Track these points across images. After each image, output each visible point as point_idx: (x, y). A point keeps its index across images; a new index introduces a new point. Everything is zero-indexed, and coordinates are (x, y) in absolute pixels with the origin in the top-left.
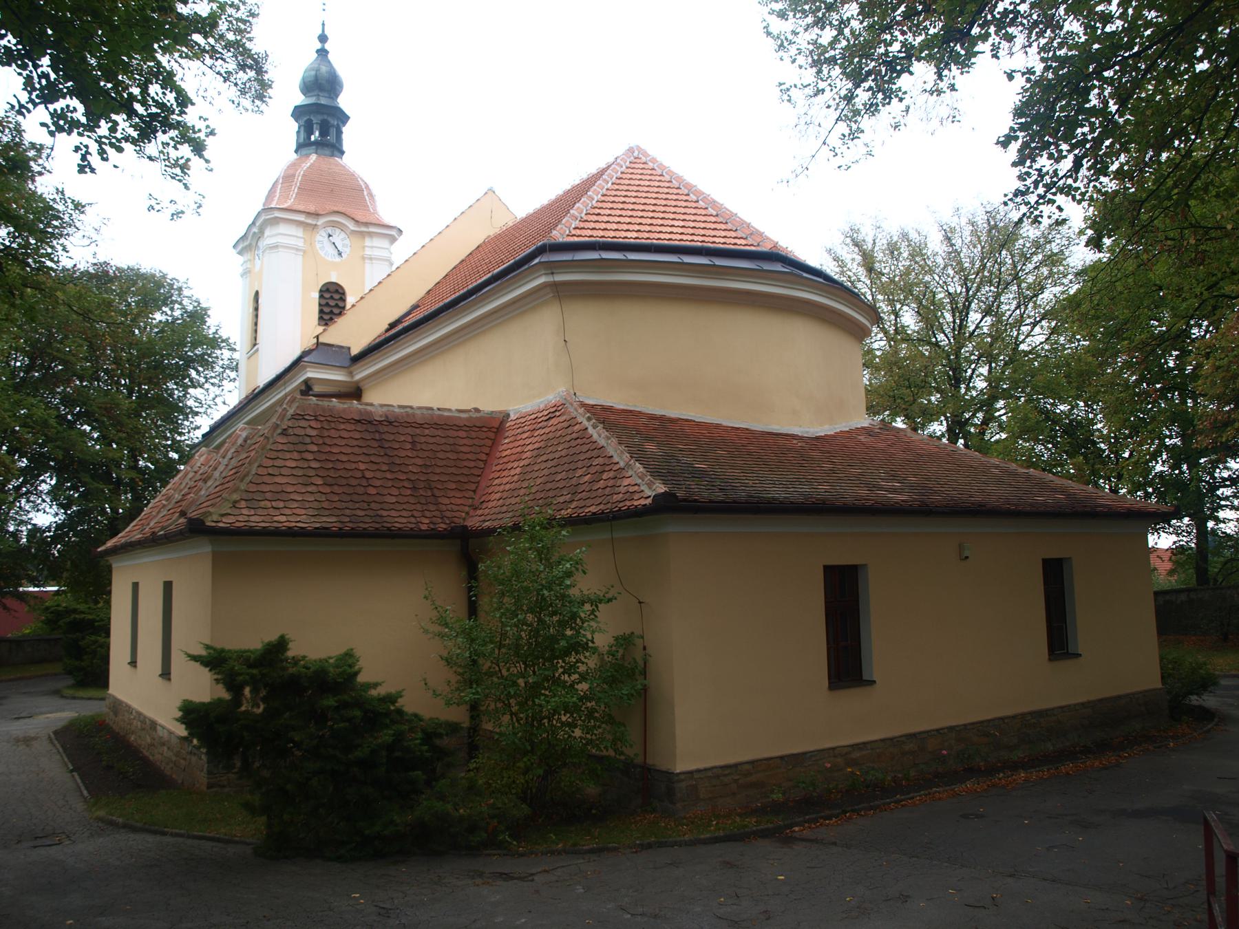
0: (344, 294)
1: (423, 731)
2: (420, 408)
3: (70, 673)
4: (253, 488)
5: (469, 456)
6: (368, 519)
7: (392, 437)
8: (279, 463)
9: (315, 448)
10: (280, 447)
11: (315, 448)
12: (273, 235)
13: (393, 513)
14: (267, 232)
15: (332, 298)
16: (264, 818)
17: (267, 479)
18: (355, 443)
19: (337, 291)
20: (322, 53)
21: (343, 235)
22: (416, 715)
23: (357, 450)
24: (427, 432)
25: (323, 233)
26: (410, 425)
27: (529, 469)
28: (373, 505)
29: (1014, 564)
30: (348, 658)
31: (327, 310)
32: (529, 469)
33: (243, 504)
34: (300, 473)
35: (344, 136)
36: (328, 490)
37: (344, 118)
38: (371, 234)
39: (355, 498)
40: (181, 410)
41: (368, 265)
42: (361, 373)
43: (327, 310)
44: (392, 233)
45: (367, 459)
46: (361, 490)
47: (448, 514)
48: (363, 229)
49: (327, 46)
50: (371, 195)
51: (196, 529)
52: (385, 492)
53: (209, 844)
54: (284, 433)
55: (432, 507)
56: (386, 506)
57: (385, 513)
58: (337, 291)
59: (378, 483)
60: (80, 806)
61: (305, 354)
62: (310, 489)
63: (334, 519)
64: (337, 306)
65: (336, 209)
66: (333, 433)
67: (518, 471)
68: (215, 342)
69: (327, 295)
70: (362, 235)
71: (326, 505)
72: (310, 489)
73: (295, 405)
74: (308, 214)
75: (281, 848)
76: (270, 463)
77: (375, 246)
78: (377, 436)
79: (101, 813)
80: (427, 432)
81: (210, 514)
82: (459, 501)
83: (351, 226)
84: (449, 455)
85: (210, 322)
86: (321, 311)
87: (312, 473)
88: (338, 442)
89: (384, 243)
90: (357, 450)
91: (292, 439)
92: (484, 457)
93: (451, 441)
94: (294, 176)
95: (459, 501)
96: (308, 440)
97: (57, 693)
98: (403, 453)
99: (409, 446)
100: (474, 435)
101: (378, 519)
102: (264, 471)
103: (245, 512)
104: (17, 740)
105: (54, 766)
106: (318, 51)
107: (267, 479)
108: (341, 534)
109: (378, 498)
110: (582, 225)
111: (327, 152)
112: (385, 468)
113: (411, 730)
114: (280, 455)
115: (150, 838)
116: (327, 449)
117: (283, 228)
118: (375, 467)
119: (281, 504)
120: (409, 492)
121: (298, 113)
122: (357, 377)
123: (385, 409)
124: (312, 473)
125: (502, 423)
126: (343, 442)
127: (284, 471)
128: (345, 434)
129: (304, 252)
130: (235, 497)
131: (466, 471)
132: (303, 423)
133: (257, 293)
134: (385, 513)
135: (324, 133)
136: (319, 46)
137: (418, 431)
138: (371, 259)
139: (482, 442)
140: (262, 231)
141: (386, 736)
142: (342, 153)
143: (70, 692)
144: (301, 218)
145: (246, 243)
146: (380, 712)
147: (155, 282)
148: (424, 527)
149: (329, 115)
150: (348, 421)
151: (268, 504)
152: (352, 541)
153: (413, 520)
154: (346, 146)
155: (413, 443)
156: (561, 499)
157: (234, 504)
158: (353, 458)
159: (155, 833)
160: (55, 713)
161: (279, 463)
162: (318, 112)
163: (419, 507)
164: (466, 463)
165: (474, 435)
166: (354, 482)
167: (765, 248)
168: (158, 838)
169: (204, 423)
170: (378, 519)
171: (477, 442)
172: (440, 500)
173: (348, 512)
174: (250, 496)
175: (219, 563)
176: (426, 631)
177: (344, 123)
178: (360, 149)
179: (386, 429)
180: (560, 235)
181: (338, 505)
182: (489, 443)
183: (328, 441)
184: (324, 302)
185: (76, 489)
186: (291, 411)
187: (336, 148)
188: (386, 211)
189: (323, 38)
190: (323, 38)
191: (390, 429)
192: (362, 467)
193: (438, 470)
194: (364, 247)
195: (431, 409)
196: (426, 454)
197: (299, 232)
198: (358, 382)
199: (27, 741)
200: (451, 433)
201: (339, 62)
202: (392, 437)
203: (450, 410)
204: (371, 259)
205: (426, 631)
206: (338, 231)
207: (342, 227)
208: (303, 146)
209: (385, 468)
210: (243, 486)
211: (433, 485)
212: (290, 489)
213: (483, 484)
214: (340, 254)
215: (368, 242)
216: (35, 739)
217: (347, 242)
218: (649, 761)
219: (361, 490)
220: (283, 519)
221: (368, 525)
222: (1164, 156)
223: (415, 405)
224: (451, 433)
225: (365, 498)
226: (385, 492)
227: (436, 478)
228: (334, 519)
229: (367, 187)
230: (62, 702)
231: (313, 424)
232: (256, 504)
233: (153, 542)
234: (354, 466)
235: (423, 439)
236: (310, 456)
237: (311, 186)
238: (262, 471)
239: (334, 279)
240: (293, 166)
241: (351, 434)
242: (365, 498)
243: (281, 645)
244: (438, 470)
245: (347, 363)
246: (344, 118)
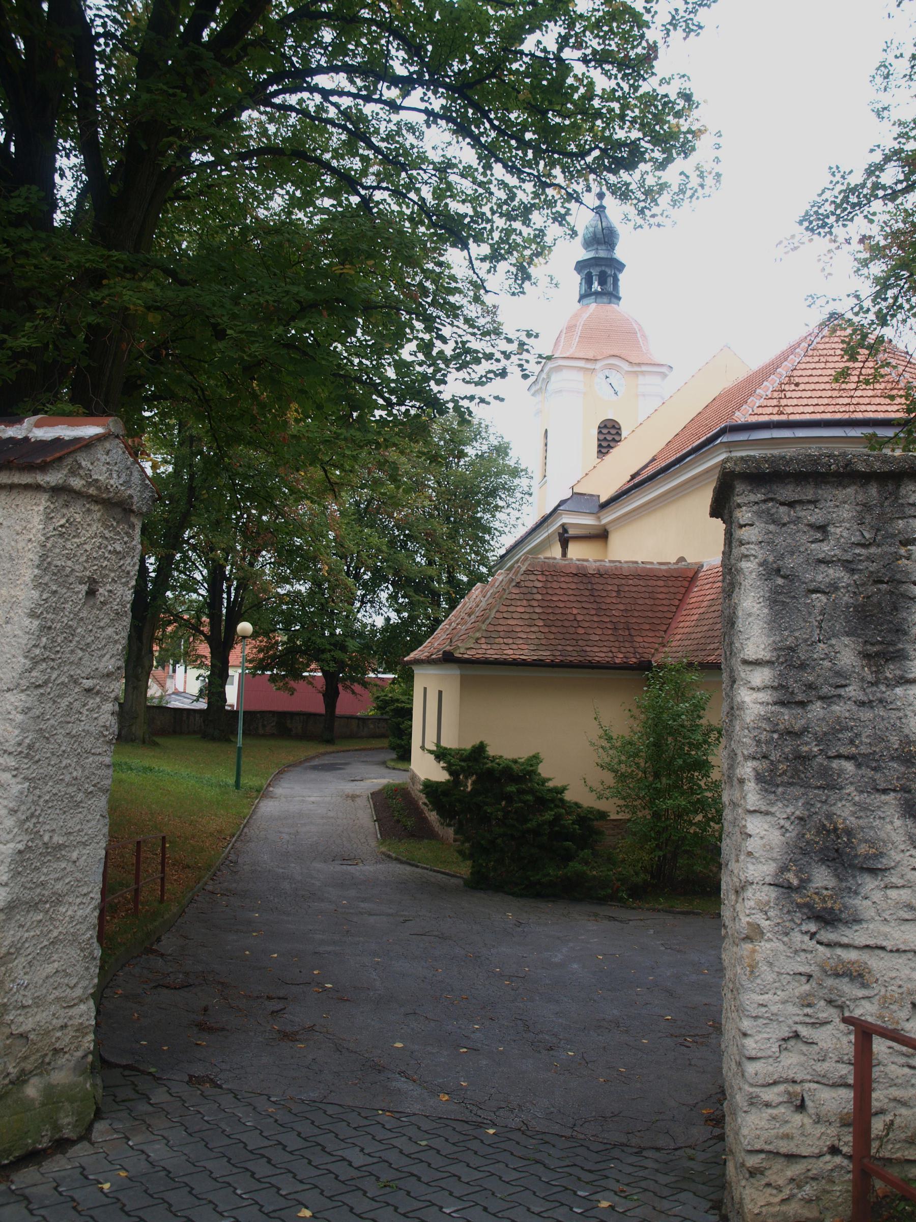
1: (578, 815)
2: (626, 562)
3: (393, 749)
4: (492, 628)
5: (664, 602)
6: (575, 654)
7: (601, 587)
8: (511, 609)
9: (539, 597)
10: (514, 596)
11: (539, 597)
13: (596, 649)
16: (469, 863)
17: (501, 622)
18: (571, 592)
19: (614, 427)
22: (576, 804)
23: (572, 598)
24: (631, 582)
26: (617, 576)
27: (702, 617)
28: (580, 643)
30: (535, 759)
31: (604, 444)
32: (702, 617)
33: (483, 640)
34: (527, 616)
35: (620, 283)
36: (546, 630)
37: (619, 266)
38: (643, 373)
39: (567, 636)
40: (488, 530)
42: (607, 518)
43: (604, 444)
44: (662, 370)
45: (579, 605)
46: (572, 630)
47: (640, 650)
48: (636, 369)
50: (644, 336)
51: (448, 658)
52: (591, 631)
53: (440, 876)
54: (518, 585)
55: (627, 645)
56: (589, 643)
57: (588, 649)
58: (614, 427)
59: (586, 625)
60: (373, 843)
61: (562, 503)
62: (533, 629)
63: (548, 653)
64: (614, 440)
66: (555, 585)
67: (695, 617)
68: (515, 473)
69: (605, 431)
71: (543, 642)
72: (533, 629)
73: (526, 564)
75: (480, 883)
76: (505, 609)
77: (648, 383)
78: (589, 587)
79: (384, 849)
80: (631, 582)
81: (459, 647)
82: (651, 640)
83: (626, 367)
84: (647, 601)
85: (511, 453)
86: (600, 446)
87: (535, 616)
88: (558, 592)
89: (657, 380)
90: (572, 598)
91: (522, 590)
92: (677, 602)
93: (650, 589)
94: (575, 326)
95: (651, 640)
96: (535, 591)
97: (384, 763)
98: (608, 600)
99: (614, 594)
100: (670, 584)
101: (583, 654)
102: (501, 616)
103: (484, 646)
104: (348, 796)
105: (365, 816)
107: (501, 622)
108: (552, 665)
109: (586, 637)
110: (765, 403)
111: (605, 299)
112: (593, 612)
113: (568, 813)
114: (513, 603)
115: (408, 868)
116: (549, 597)
117: (565, 374)
118: (585, 611)
119: (510, 641)
120: (610, 632)
121: (581, 266)
122: (604, 522)
123: (598, 564)
124: (535, 616)
125: (697, 573)
126: (562, 592)
127: (515, 615)
128: (564, 586)
130: (478, 635)
131: (659, 615)
132: (532, 577)
134: (588, 649)
135: (602, 283)
137: (623, 582)
139: (676, 590)
140: (549, 377)
141: (548, 816)
142: (619, 299)
143: (392, 764)
144: (581, 364)
145: (538, 387)
146: (552, 799)
148: (617, 661)
149: (606, 266)
150: (567, 575)
151: (501, 641)
152: (563, 669)
153: (610, 655)
154: (622, 292)
155: (618, 591)
156: (712, 646)
157: (477, 641)
158: (569, 605)
159: (413, 865)
160: (378, 778)
161: (511, 609)
162: (597, 265)
163: (617, 644)
164: (660, 608)
165: (670, 584)
166: (567, 624)
168: (414, 868)
169: (508, 541)
170: (583, 654)
171: (672, 590)
172: (636, 639)
173: (560, 647)
174: (489, 634)
175: (465, 683)
176: (592, 744)
177: (621, 271)
179: (597, 580)
180: (741, 417)
181: (553, 642)
182: (683, 590)
183: (550, 591)
184: (602, 437)
186: (524, 568)
188: (657, 350)
191: (601, 580)
192: (575, 611)
193: (636, 614)
195: (636, 563)
196: (628, 600)
197: (578, 376)
198: (604, 525)
199: (353, 797)
200: (651, 583)
202: (601, 587)
203: (652, 563)
205: (592, 744)
206: (614, 372)
209: (593, 612)
210: (484, 627)
211: (631, 626)
212: (518, 629)
213: (673, 625)
215: (641, 380)
216: (358, 796)
219: (572, 630)
220: (511, 652)
221: (574, 658)
223: (623, 560)
224: (651, 583)
225: (574, 636)
226: (591, 631)
227: (634, 620)
228: (548, 653)
229: (641, 329)
230: (387, 771)
231: (540, 578)
232: (492, 640)
233: (429, 662)
234: (568, 611)
235: (627, 588)
236: (535, 604)
237: (590, 335)
238: (499, 615)
240: (576, 316)
241: (569, 586)
242: (574, 636)
243: (480, 749)
244: (636, 614)
245: (596, 509)
246: (619, 266)
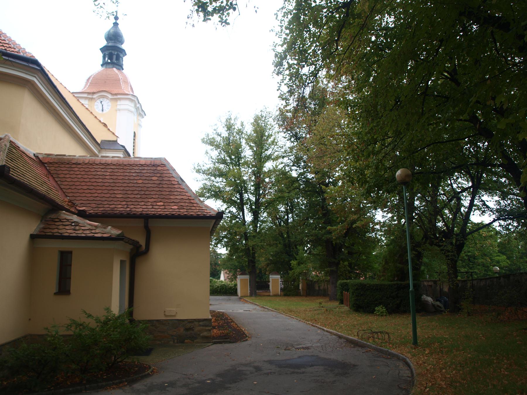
20: (116, 24)
21: (108, 101)
25: (99, 101)
29: (140, 223)
38: (120, 99)
48: (115, 97)
49: (118, 22)
65: (101, 90)
70: (116, 100)
74: (89, 93)
83: (110, 96)
133: (135, 133)
136: (114, 21)
138: (119, 110)
144: (85, 95)
162: (108, 50)
167: (28, 56)
185: (353, 170)
187: (120, 66)
194: (117, 105)
201: (123, 29)
204: (119, 110)
206: (105, 99)
207: (103, 97)
208: (104, 64)
214: (103, 110)
215: (119, 102)
217: (110, 104)
218: (142, 313)
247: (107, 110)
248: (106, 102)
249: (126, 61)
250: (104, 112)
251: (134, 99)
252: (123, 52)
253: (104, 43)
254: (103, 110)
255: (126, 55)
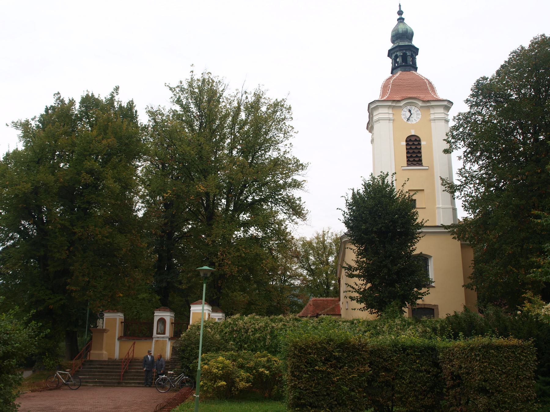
0: (420, 141)
12: (377, 115)
14: (374, 114)
15: (413, 144)
20: (401, 20)
21: (416, 109)
38: (433, 107)
41: (433, 124)
49: (403, 16)
65: (411, 96)
83: (420, 104)
106: (398, 20)
117: (381, 110)
129: (393, 120)
136: (398, 17)
144: (390, 104)
147: (68, 193)
178: (424, 66)
184: (408, 147)
188: (442, 94)
189: (400, 13)
190: (400, 13)
197: (390, 111)
201: (410, 22)
204: (434, 120)
206: (413, 107)
207: (415, 105)
208: (394, 70)
214: (408, 119)
215: (432, 111)
217: (419, 112)
222: (148, 198)
239: (413, 133)
240: (390, 78)
247: (414, 122)
248: (414, 110)
249: (419, 60)
250: (409, 122)
251: (373, 134)
252: (415, 51)
253: (390, 46)
254: (408, 119)
255: (417, 49)
